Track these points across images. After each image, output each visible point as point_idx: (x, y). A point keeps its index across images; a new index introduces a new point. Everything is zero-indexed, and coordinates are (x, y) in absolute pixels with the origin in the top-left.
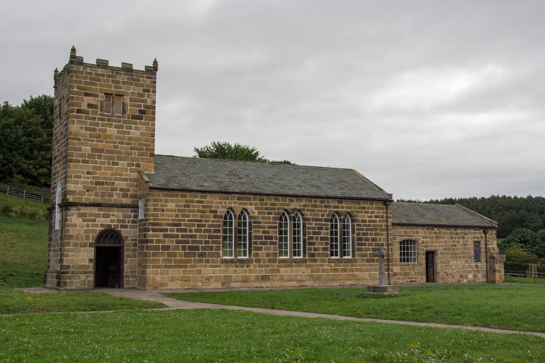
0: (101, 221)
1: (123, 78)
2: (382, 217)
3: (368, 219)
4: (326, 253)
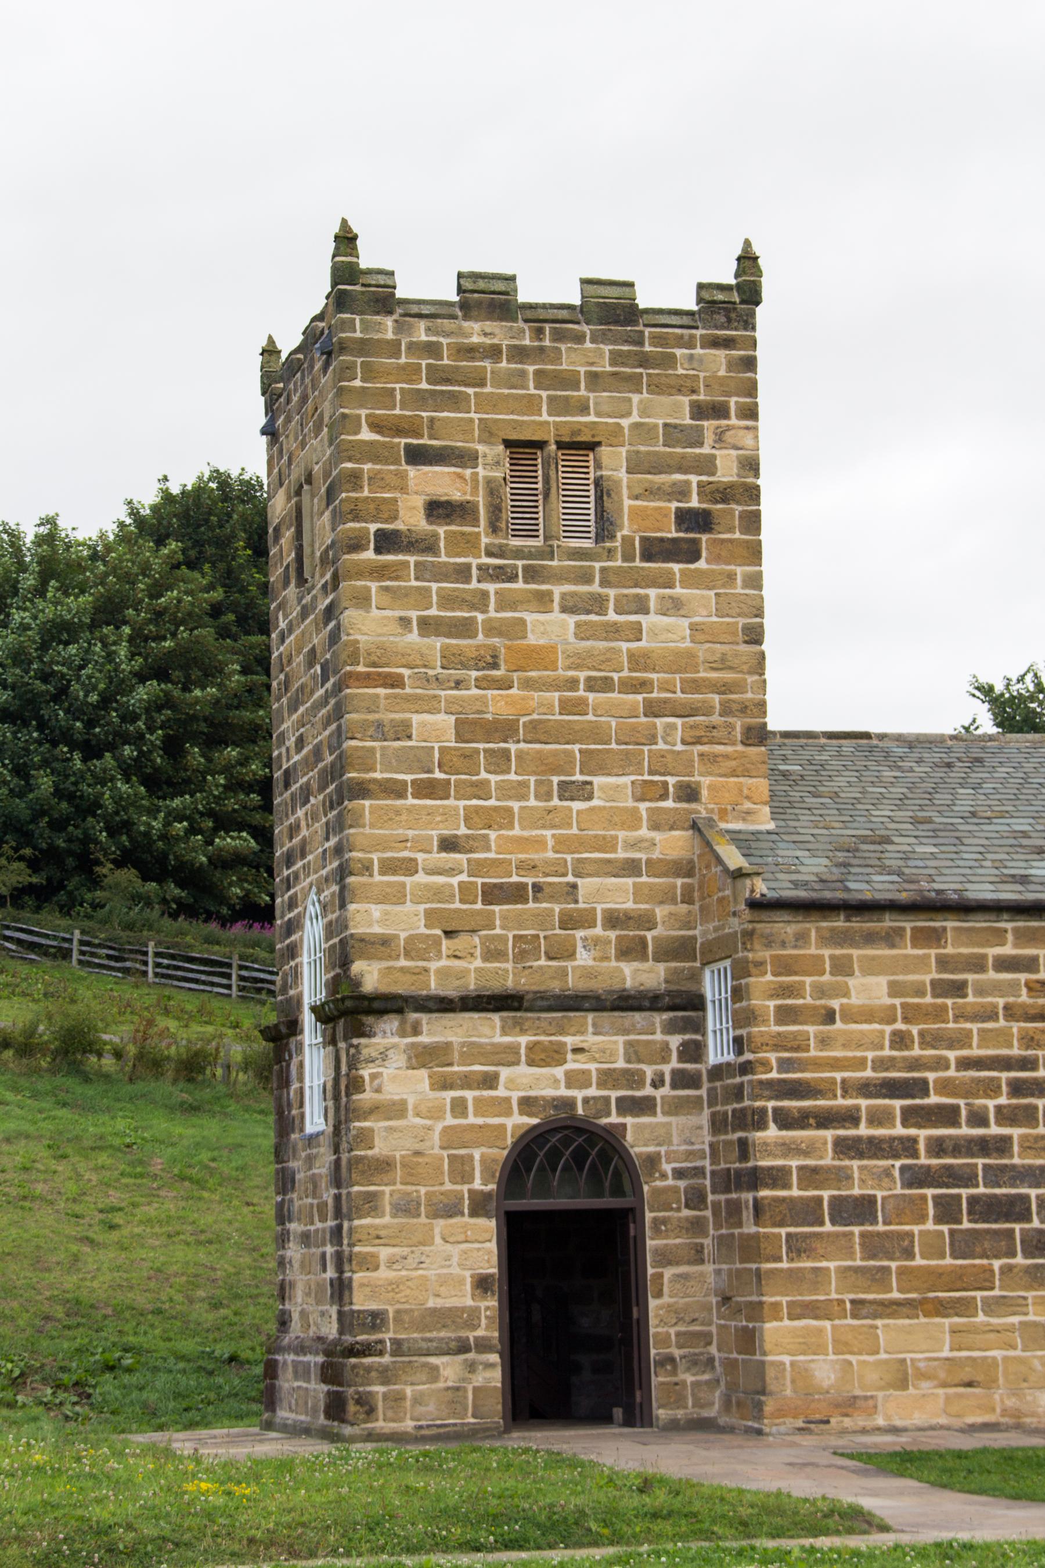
0: (521, 1080)
1: (589, 354)
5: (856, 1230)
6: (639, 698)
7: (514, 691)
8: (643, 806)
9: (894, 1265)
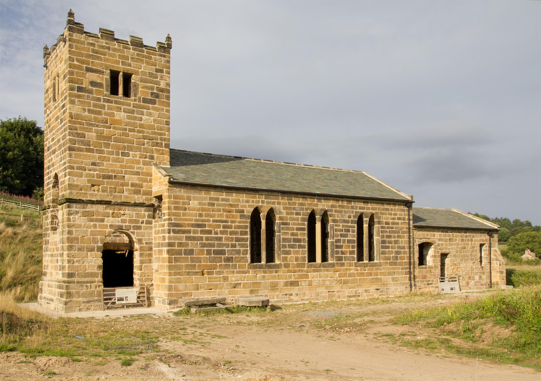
0: (109, 221)
1: (131, 52)
2: (404, 219)
3: (391, 221)
4: (353, 257)
5: (189, 256)
6: (141, 134)
7: (111, 129)
8: (141, 159)
9: (197, 264)
